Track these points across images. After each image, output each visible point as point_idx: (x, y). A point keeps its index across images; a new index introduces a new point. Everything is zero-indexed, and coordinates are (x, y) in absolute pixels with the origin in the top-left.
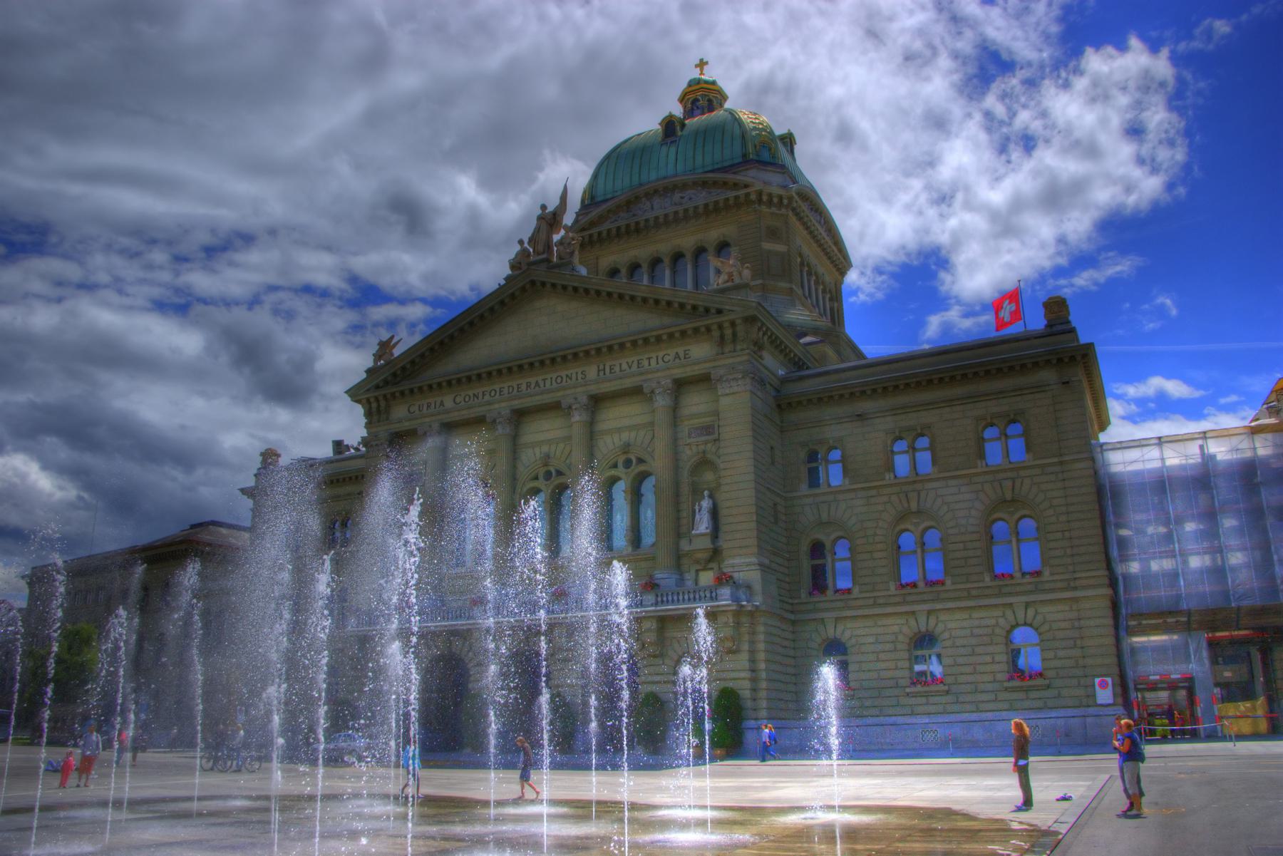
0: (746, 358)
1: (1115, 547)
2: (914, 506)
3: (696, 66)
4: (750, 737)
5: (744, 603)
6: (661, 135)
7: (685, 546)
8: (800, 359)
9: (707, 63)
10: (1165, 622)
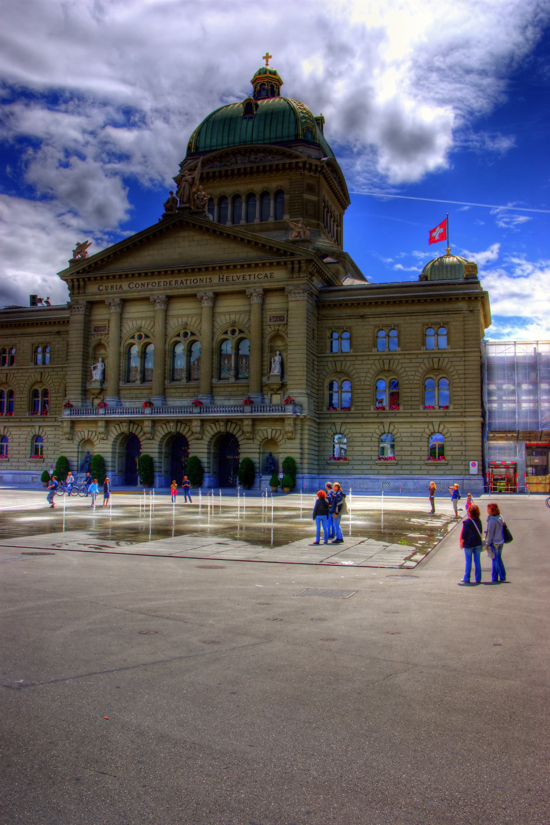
0: (305, 282)
1: (486, 395)
3: (264, 58)
4: (299, 482)
5: (299, 414)
6: (243, 110)
8: (329, 279)
9: (270, 57)
10: (506, 436)
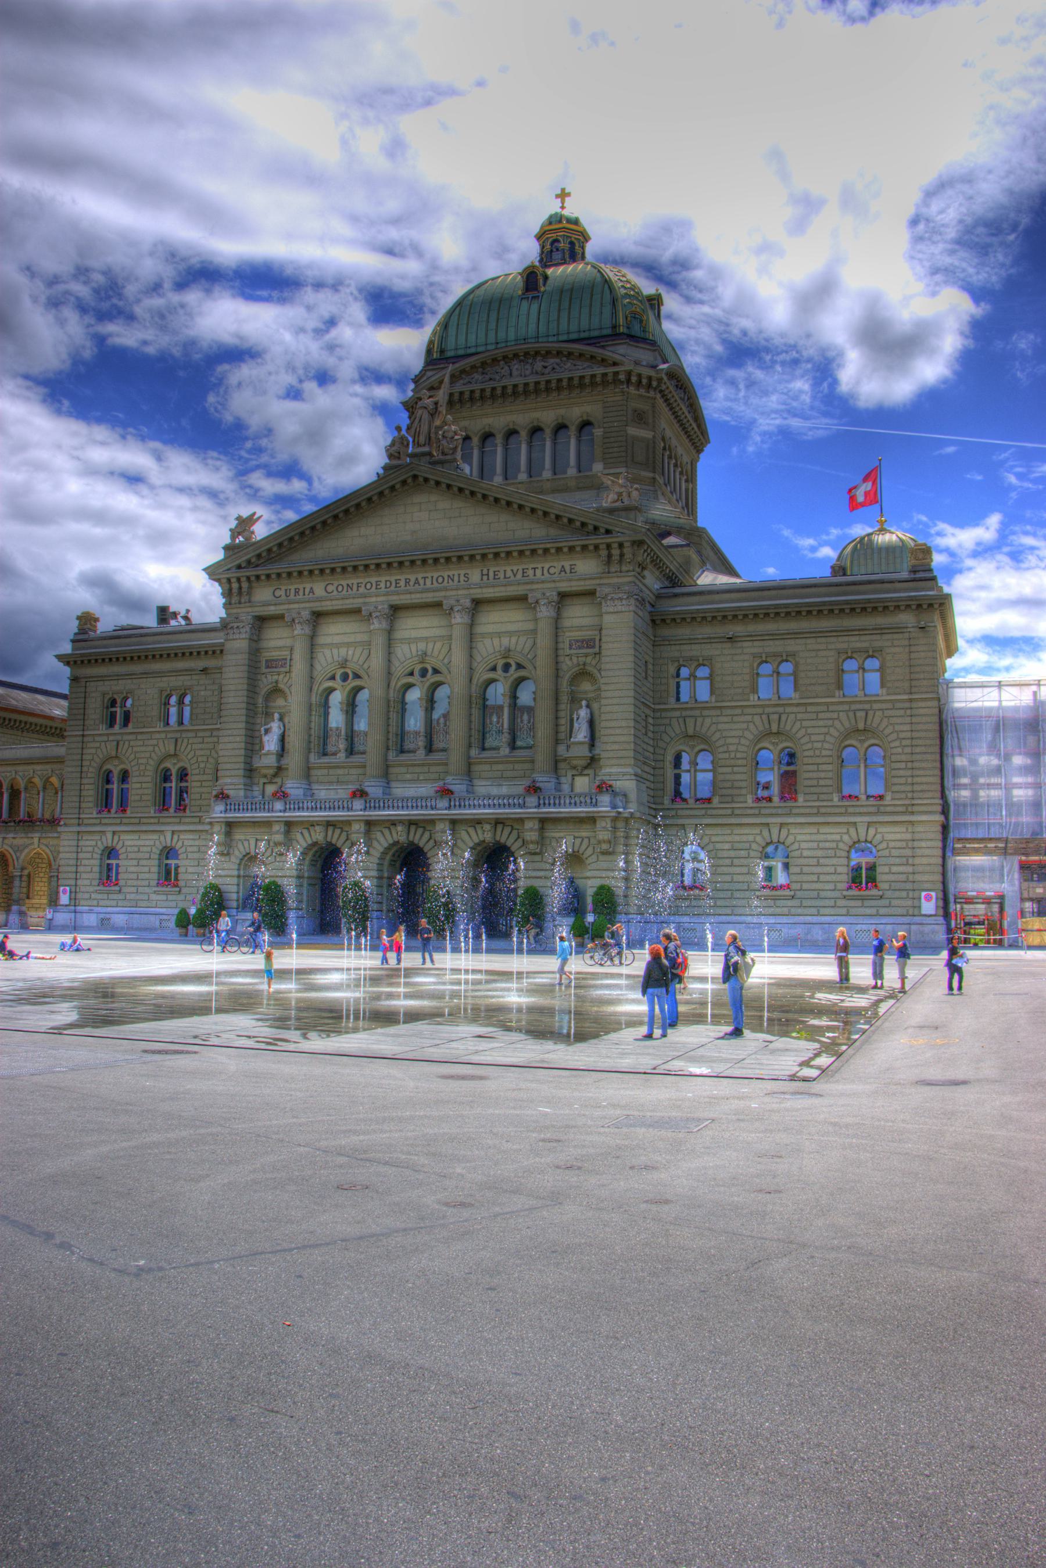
2: (774, 729)
3: (557, 196)
5: (621, 810)
6: (521, 285)
7: (561, 749)
